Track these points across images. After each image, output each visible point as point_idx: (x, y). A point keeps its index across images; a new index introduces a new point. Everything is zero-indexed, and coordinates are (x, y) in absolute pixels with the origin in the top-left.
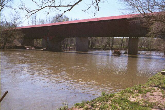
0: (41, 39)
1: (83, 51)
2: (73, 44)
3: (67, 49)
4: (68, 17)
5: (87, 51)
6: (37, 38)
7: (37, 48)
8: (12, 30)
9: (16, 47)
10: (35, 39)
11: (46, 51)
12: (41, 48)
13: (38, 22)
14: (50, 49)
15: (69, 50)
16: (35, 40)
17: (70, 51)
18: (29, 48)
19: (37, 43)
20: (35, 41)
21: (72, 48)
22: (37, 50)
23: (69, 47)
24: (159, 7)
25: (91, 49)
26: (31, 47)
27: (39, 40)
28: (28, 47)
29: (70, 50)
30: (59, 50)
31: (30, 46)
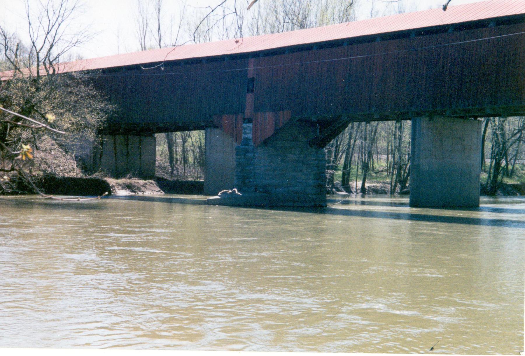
0: (196, 137)
1: (445, 206)
2: (381, 162)
3: (348, 189)
4: (302, 30)
5: (474, 206)
6: (169, 129)
7: (174, 187)
8: (35, 81)
9: (54, 185)
10: (160, 131)
11: (239, 206)
12: (194, 188)
13: (176, 28)
14: (260, 195)
15: (359, 199)
16: (160, 137)
17: (363, 203)
18: (129, 187)
19: (171, 159)
20: (161, 147)
21: (379, 185)
22: (170, 201)
23: (360, 184)
24: (15, 203)
25: (495, 189)
26: (142, 182)
27: (184, 141)
28: (121, 181)
29: (366, 199)
30: (314, 200)
31: (134, 175)
